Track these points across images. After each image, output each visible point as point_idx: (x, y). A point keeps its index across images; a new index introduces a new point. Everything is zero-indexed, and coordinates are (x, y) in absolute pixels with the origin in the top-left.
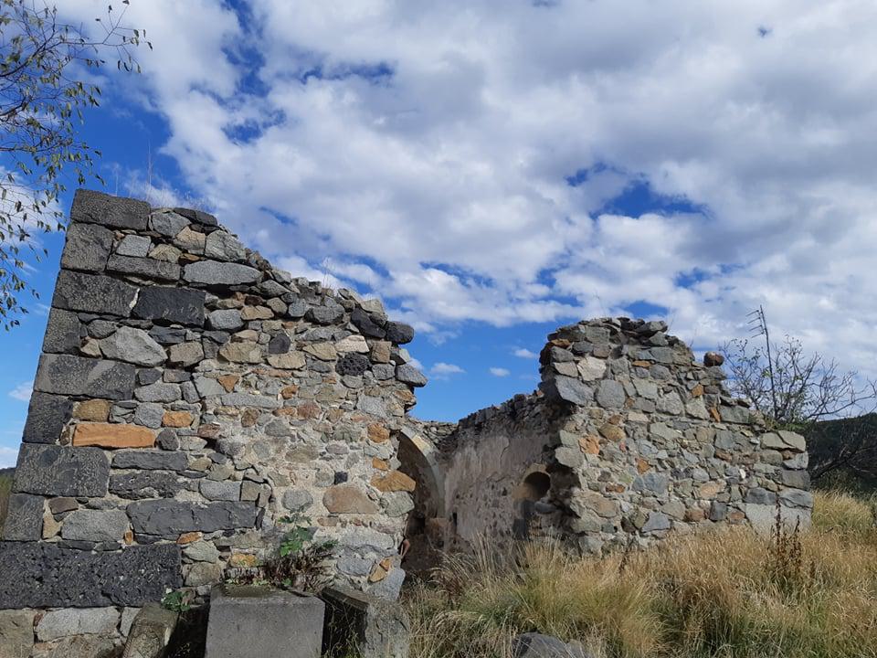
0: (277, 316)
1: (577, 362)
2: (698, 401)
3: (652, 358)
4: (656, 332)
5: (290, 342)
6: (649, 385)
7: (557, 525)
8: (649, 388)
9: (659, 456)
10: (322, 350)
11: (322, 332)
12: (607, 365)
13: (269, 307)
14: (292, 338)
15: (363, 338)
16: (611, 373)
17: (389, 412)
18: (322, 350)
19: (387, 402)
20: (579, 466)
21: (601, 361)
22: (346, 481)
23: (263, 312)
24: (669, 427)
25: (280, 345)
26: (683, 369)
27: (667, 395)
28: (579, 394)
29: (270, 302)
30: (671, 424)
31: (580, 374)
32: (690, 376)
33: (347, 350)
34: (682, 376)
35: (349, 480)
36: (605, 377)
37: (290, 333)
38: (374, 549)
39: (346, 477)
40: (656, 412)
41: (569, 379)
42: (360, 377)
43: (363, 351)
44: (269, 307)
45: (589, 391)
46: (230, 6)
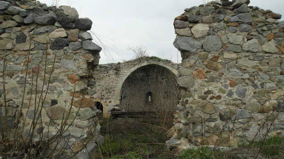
0: (19, 25)
1: (191, 27)
2: (270, 43)
3: (240, 20)
4: (242, 4)
5: (26, 37)
6: (238, 36)
7: (38, 132)
8: (238, 38)
9: (244, 77)
10: (42, 38)
11: (42, 29)
12: (210, 27)
13: (14, 20)
14: (27, 35)
15: (63, 29)
16: (212, 32)
17: (78, 67)
18: (42, 38)
19: (77, 62)
20: (192, 87)
21: (207, 25)
22: (57, 104)
23: (10, 23)
24: (250, 59)
25: (21, 39)
26: (260, 25)
27: (249, 41)
28: (192, 46)
29: (14, 17)
30: (251, 57)
31: (192, 34)
32: (265, 28)
33: (55, 37)
34: (259, 29)
35: (58, 103)
36: (209, 34)
37: (26, 32)
38: (73, 137)
39: (57, 102)
40: (239, 49)
41: (185, 37)
42: (62, 51)
43: (63, 36)
44: (14, 20)
45: (198, 43)
46: (183, 16)
